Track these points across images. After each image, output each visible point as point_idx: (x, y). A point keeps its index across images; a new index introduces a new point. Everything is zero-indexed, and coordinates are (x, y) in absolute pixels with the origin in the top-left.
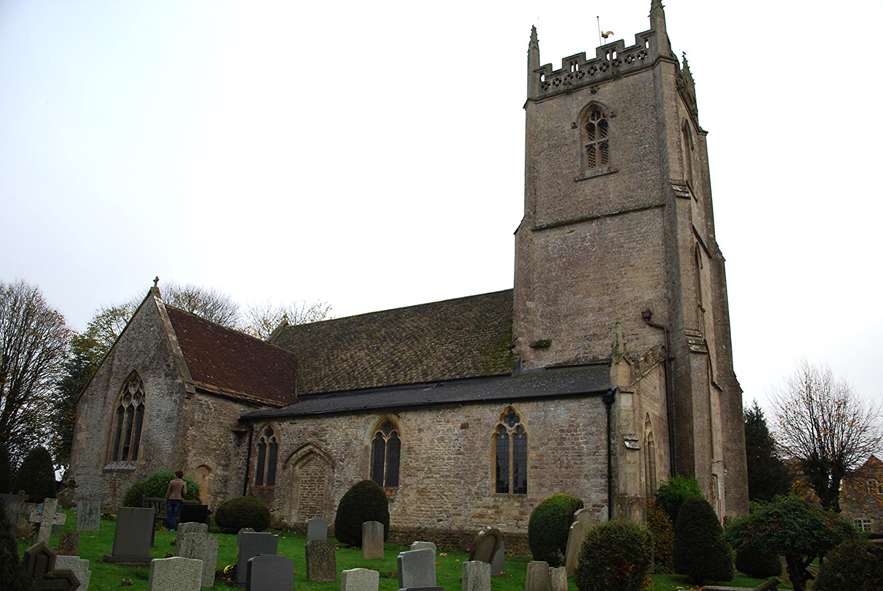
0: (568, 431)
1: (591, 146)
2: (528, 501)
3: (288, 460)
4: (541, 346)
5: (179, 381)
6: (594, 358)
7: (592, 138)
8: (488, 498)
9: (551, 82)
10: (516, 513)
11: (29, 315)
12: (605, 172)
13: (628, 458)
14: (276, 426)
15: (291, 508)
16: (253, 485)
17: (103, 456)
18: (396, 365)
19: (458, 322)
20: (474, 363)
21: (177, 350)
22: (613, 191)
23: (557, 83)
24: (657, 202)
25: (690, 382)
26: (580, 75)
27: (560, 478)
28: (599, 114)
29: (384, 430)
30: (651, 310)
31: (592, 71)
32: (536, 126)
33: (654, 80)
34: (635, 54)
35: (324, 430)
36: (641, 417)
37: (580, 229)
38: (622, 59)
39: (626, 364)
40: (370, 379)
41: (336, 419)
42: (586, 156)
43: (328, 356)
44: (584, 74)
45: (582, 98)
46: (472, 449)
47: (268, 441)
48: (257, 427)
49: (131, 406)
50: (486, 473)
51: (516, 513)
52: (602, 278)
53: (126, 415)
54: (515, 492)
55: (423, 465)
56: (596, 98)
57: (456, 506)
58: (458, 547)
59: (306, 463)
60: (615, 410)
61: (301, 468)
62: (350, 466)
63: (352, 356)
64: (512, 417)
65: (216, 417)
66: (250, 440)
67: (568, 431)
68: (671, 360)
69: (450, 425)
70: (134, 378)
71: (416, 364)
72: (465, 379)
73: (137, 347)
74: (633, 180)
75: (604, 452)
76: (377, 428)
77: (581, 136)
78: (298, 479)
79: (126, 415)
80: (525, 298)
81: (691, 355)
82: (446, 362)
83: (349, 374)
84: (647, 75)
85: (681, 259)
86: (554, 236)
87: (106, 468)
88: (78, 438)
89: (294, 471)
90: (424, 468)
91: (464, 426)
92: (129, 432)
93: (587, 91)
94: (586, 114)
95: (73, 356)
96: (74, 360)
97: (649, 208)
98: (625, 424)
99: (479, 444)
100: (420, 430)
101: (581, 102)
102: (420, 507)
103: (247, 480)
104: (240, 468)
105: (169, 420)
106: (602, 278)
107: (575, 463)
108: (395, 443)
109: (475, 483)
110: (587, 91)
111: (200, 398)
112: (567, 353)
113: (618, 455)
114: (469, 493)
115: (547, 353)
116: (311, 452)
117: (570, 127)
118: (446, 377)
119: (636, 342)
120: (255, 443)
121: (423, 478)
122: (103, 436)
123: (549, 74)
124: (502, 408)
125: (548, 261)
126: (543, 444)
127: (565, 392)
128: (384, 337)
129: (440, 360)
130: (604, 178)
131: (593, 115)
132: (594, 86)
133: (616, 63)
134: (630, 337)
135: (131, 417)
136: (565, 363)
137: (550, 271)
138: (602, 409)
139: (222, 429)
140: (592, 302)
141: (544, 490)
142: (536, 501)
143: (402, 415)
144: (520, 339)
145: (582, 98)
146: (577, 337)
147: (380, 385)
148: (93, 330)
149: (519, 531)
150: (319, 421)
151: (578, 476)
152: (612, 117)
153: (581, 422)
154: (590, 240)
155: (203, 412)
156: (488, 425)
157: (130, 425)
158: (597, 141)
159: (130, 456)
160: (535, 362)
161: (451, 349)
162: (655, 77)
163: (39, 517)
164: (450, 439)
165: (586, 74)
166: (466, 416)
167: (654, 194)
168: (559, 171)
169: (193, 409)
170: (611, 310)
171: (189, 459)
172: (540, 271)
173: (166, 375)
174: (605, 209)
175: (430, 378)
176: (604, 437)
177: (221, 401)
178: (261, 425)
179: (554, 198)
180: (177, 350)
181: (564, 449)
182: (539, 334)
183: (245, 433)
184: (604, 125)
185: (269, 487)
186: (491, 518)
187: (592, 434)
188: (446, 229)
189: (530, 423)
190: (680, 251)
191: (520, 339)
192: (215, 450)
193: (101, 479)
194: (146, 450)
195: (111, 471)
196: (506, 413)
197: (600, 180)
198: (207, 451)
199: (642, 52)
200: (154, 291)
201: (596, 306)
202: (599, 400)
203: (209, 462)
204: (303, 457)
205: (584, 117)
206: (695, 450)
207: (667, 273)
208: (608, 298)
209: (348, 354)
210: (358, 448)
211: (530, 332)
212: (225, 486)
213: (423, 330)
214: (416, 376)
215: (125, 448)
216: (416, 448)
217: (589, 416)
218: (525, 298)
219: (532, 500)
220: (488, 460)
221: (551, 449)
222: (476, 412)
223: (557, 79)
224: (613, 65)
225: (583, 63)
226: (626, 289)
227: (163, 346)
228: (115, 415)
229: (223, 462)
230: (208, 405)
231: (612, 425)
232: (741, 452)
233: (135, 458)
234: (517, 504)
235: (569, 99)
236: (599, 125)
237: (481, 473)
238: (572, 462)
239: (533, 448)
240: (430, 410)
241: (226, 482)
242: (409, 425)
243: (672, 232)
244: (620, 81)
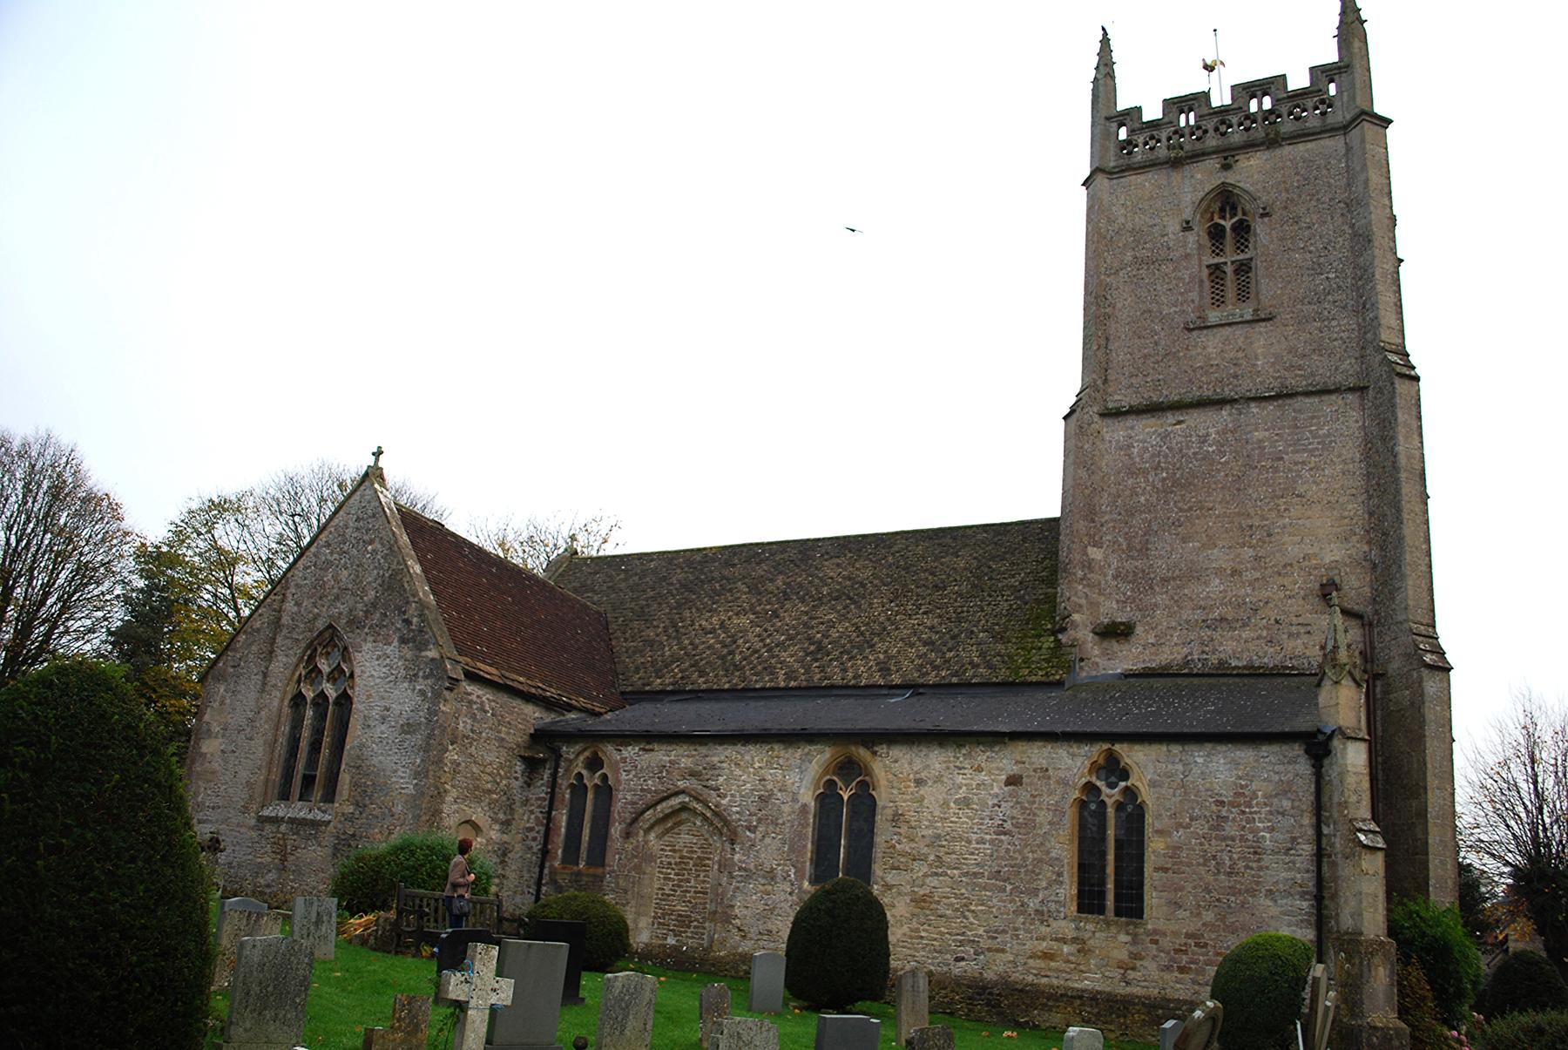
0: (1232, 804)
1: (1217, 267)
2: (1148, 933)
3: (635, 820)
4: (1115, 632)
5: (432, 653)
6: (1221, 663)
7: (1218, 249)
8: (1063, 923)
9: (1141, 140)
10: (1122, 955)
11: (57, 499)
12: (1249, 318)
13: (1364, 865)
14: (610, 751)
15: (638, 914)
16: (557, 864)
17: (259, 789)
18: (820, 648)
19: (933, 574)
20: (982, 655)
21: (425, 592)
22: (1263, 354)
24: (1352, 382)
25: (1422, 723)
27: (1215, 894)
28: (1234, 209)
29: (838, 775)
31: (1223, 128)
32: (1110, 221)
33: (1346, 154)
34: (1310, 103)
35: (714, 767)
37: (1194, 419)
38: (1284, 110)
39: (1352, 684)
40: (770, 670)
41: (739, 747)
42: (1207, 284)
43: (672, 620)
44: (1206, 132)
45: (1202, 179)
46: (1028, 825)
47: (592, 780)
48: (568, 751)
49: (322, 695)
50: (1059, 874)
51: (1122, 955)
52: (1239, 514)
53: (309, 713)
54: (1118, 913)
55: (925, 850)
56: (1230, 177)
57: (993, 934)
58: (999, 1014)
59: (672, 828)
60: (1331, 772)
61: (659, 837)
62: (768, 840)
63: (722, 624)
64: (1113, 769)
65: (493, 726)
66: (554, 775)
67: (1232, 804)
68: (1377, 676)
69: (983, 776)
70: (328, 640)
71: (861, 648)
72: (970, 685)
73: (336, 579)
74: (1304, 336)
75: (1307, 849)
76: (826, 772)
77: (1200, 247)
78: (650, 858)
79: (309, 713)
80: (1085, 540)
81: (1425, 672)
82: (923, 650)
83: (723, 658)
84: (1334, 144)
85: (1404, 491)
86: (1145, 430)
87: (266, 813)
88: (204, 750)
89: (646, 842)
90: (926, 856)
91: (1013, 781)
92: (315, 747)
93: (1213, 163)
94: (1209, 206)
95: (141, 584)
96: (141, 590)
97: (1337, 390)
98: (1353, 799)
99: (1043, 817)
100: (919, 782)
101: (1201, 182)
102: (917, 930)
103: (545, 853)
104: (531, 829)
105: (408, 728)
106: (1239, 514)
107: (1247, 867)
108: (865, 805)
109: (1035, 892)
110: (1213, 163)
111: (469, 689)
112: (1166, 649)
113: (1339, 859)
114: (1022, 910)
115: (1127, 646)
116: (684, 808)
117: (1178, 228)
118: (932, 679)
119: (1305, 638)
120: (563, 783)
121: (925, 875)
122: (259, 748)
123: (1137, 125)
124: (1095, 751)
125: (1132, 474)
126: (1180, 826)
127: (1221, 729)
128: (785, 593)
129: (912, 645)
130: (1246, 328)
131: (1222, 210)
135: (321, 717)
137: (1134, 493)
138: (1304, 767)
139: (503, 752)
140: (1219, 557)
141: (1181, 914)
142: (1165, 934)
143: (882, 749)
145: (1202, 179)
146: (1187, 622)
147: (792, 684)
148: (180, 536)
149: (1128, 990)
150: (703, 750)
151: (1253, 892)
152: (1262, 216)
153: (1260, 788)
154: (1216, 442)
155: (474, 717)
156: (1063, 782)
157: (318, 732)
158: (1230, 257)
159: (318, 793)
160: (1102, 662)
161: (937, 626)
162: (1349, 149)
163: (466, 987)
164: (983, 804)
165: (1211, 131)
166: (1017, 762)
167: (1346, 365)
168: (1154, 307)
169: (458, 710)
170: (1258, 575)
171: (446, 808)
172: (1113, 491)
173: (403, 641)
174: (1246, 386)
175: (896, 679)
176: (1307, 820)
177: (504, 698)
178: (578, 747)
179: (1145, 356)
180: (425, 592)
181: (1224, 839)
182: (1110, 610)
183: (543, 761)
184: (1242, 230)
185: (591, 871)
186: (1069, 961)
187: (1283, 814)
188: (945, 403)
189: (1153, 784)
190: (1403, 475)
191: (1076, 617)
192: (489, 792)
193: (254, 834)
194: (356, 785)
195: (276, 820)
196: (1101, 761)
197: (1239, 331)
198: (475, 793)
199: (1323, 102)
200: (373, 475)
201: (1228, 566)
202: (1297, 750)
203: (479, 815)
204: (666, 817)
205: (1206, 211)
206: (1431, 850)
207: (1371, 514)
208: (1251, 552)
209: (715, 620)
210: (786, 808)
211: (1094, 605)
212: (503, 862)
213: (863, 585)
214: (864, 670)
215: (305, 777)
216: (910, 815)
217: (1276, 778)
218: (1085, 540)
219: (1155, 932)
220: (1063, 849)
221: (1196, 835)
222: (1038, 754)
225: (1205, 111)
226: (1286, 538)
227: (394, 583)
228: (286, 710)
229: (501, 816)
230: (482, 703)
231: (1325, 799)
233: (330, 796)
234: (1123, 938)
235: (1176, 177)
236: (1234, 228)
237: (1048, 872)
238: (1241, 864)
239: (1159, 832)
240: (941, 745)
241: (504, 854)
242: (893, 771)
243: (1383, 439)
244: (1278, 152)
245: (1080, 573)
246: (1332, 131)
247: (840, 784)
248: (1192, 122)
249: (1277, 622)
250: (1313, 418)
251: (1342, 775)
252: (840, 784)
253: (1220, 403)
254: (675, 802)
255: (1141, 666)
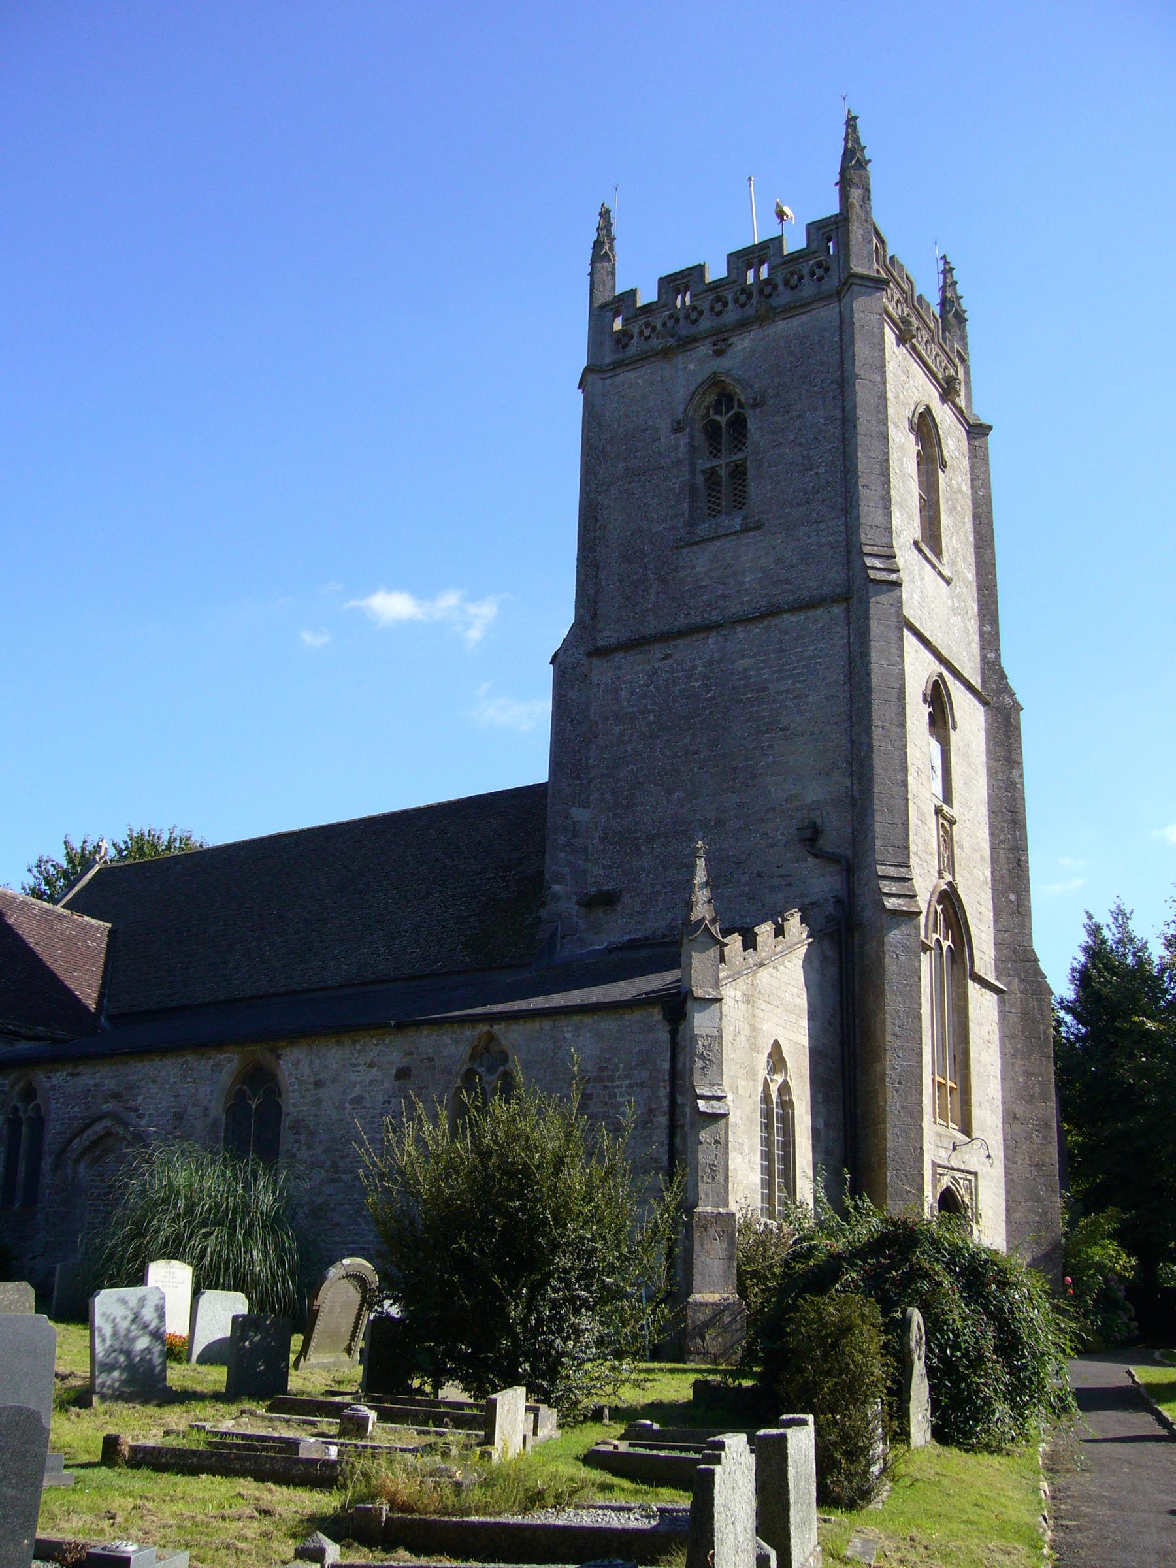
4: (607, 900)
9: (636, 331)
23: (647, 332)
26: (694, 316)
30: (818, 821)
31: (718, 307)
36: (754, 1048)
38: (779, 281)
44: (701, 313)
55: (323, 1157)
100: (318, 1084)
110: (704, 349)
116: (108, 1134)
132: (720, 341)
133: (766, 288)
134: (776, 882)
136: (647, 938)
144: (557, 888)
145: (695, 366)
158: (722, 463)
165: (707, 314)
174: (734, 608)
182: (598, 877)
184: (739, 424)
191: (557, 888)
204: (94, 1144)
208: (735, 798)
223: (647, 325)
224: (761, 292)
231: (680, 1066)
232: (1047, 1125)
236: (730, 424)
245: (562, 839)
246: (823, 298)
247: (249, 1093)
248: (688, 303)
249: (759, 875)
250: (797, 638)
251: (694, 1038)
252: (249, 1093)
253: (706, 628)
254: (99, 1128)
255: (627, 938)
